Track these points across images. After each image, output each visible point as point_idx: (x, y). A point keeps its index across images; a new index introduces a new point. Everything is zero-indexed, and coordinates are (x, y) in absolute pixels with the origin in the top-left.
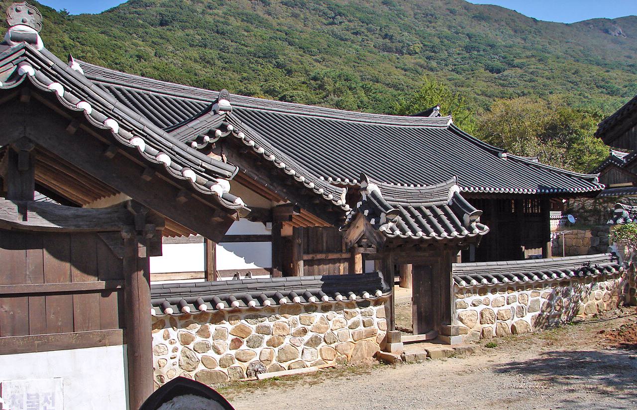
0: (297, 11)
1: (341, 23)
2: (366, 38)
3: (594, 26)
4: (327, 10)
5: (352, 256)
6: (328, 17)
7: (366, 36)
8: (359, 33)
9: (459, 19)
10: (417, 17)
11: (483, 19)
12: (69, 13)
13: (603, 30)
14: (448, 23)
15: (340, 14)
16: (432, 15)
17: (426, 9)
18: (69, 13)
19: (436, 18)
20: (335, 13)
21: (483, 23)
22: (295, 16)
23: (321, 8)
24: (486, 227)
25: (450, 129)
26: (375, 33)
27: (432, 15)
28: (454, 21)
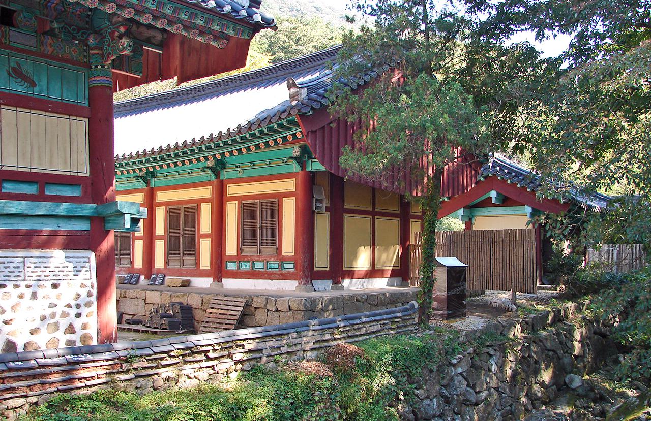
10: (282, 10)
27: (298, 11)
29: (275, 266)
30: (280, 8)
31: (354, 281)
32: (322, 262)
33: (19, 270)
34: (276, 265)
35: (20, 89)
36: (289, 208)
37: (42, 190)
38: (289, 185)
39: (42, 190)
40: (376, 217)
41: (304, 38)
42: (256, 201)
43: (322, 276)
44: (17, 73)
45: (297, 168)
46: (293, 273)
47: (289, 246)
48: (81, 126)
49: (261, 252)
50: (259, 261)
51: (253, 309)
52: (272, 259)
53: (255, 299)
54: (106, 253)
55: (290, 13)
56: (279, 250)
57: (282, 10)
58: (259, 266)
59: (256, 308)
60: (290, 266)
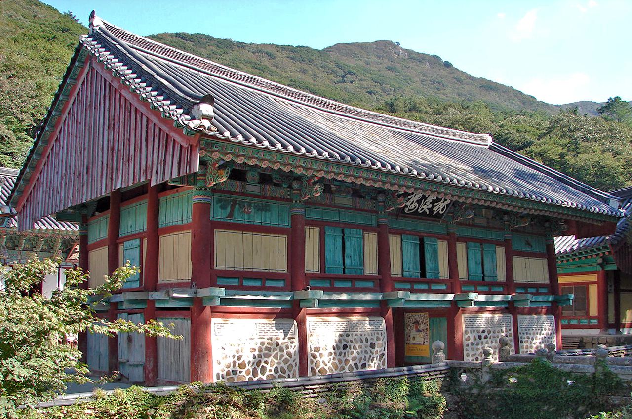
0: (306, 67)
1: (351, 82)
2: (381, 98)
3: (582, 108)
4: (336, 69)
5: (315, 225)
6: (337, 75)
7: (381, 96)
8: (373, 93)
9: (467, 88)
10: (424, 83)
11: (491, 89)
12: (75, 16)
13: (593, 112)
14: (456, 91)
15: (350, 73)
16: (439, 83)
17: (432, 77)
18: (75, 16)
19: (443, 86)
20: (345, 72)
21: (492, 93)
22: (304, 71)
23: (331, 66)
24: (420, 212)
25: (490, 148)
26: (389, 94)
27: (439, 83)
28: (463, 89)
29: (584, 322)
30: (422, 82)
31: (625, 329)
32: (612, 320)
33: (383, 333)
34: (585, 321)
35: (529, 249)
36: (593, 291)
37: (353, 285)
38: (594, 278)
39: (537, 291)
40: (467, 280)
41: (479, 127)
42: (571, 286)
43: (611, 326)
44: (528, 244)
45: (599, 268)
46: (597, 325)
47: (594, 310)
48: (545, 261)
49: (575, 314)
50: (574, 319)
51: (584, 344)
52: (583, 318)
53: (585, 338)
54: (205, 334)
55: (432, 86)
56: (587, 312)
57: (424, 83)
58: (574, 322)
59: (585, 343)
60: (595, 322)
